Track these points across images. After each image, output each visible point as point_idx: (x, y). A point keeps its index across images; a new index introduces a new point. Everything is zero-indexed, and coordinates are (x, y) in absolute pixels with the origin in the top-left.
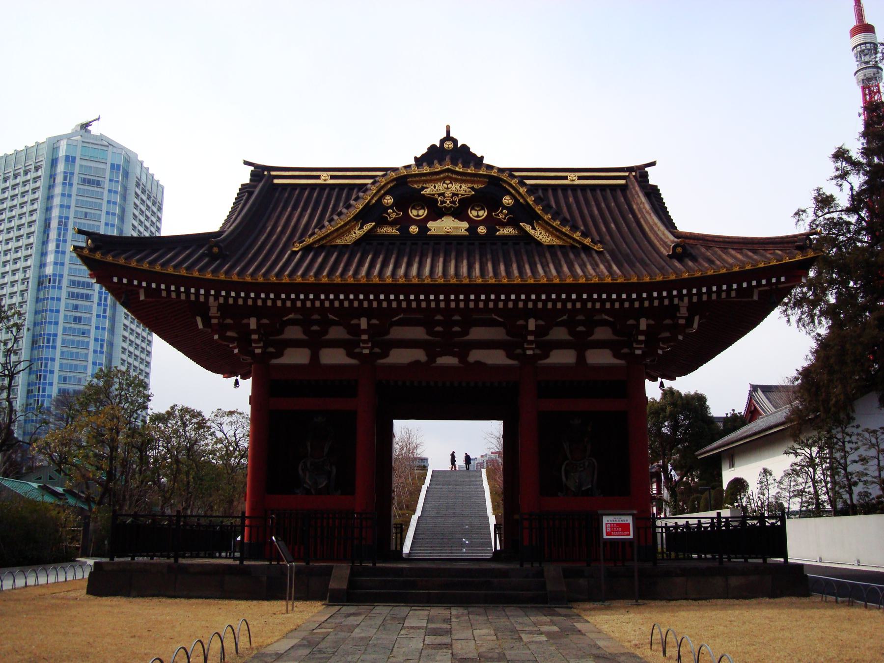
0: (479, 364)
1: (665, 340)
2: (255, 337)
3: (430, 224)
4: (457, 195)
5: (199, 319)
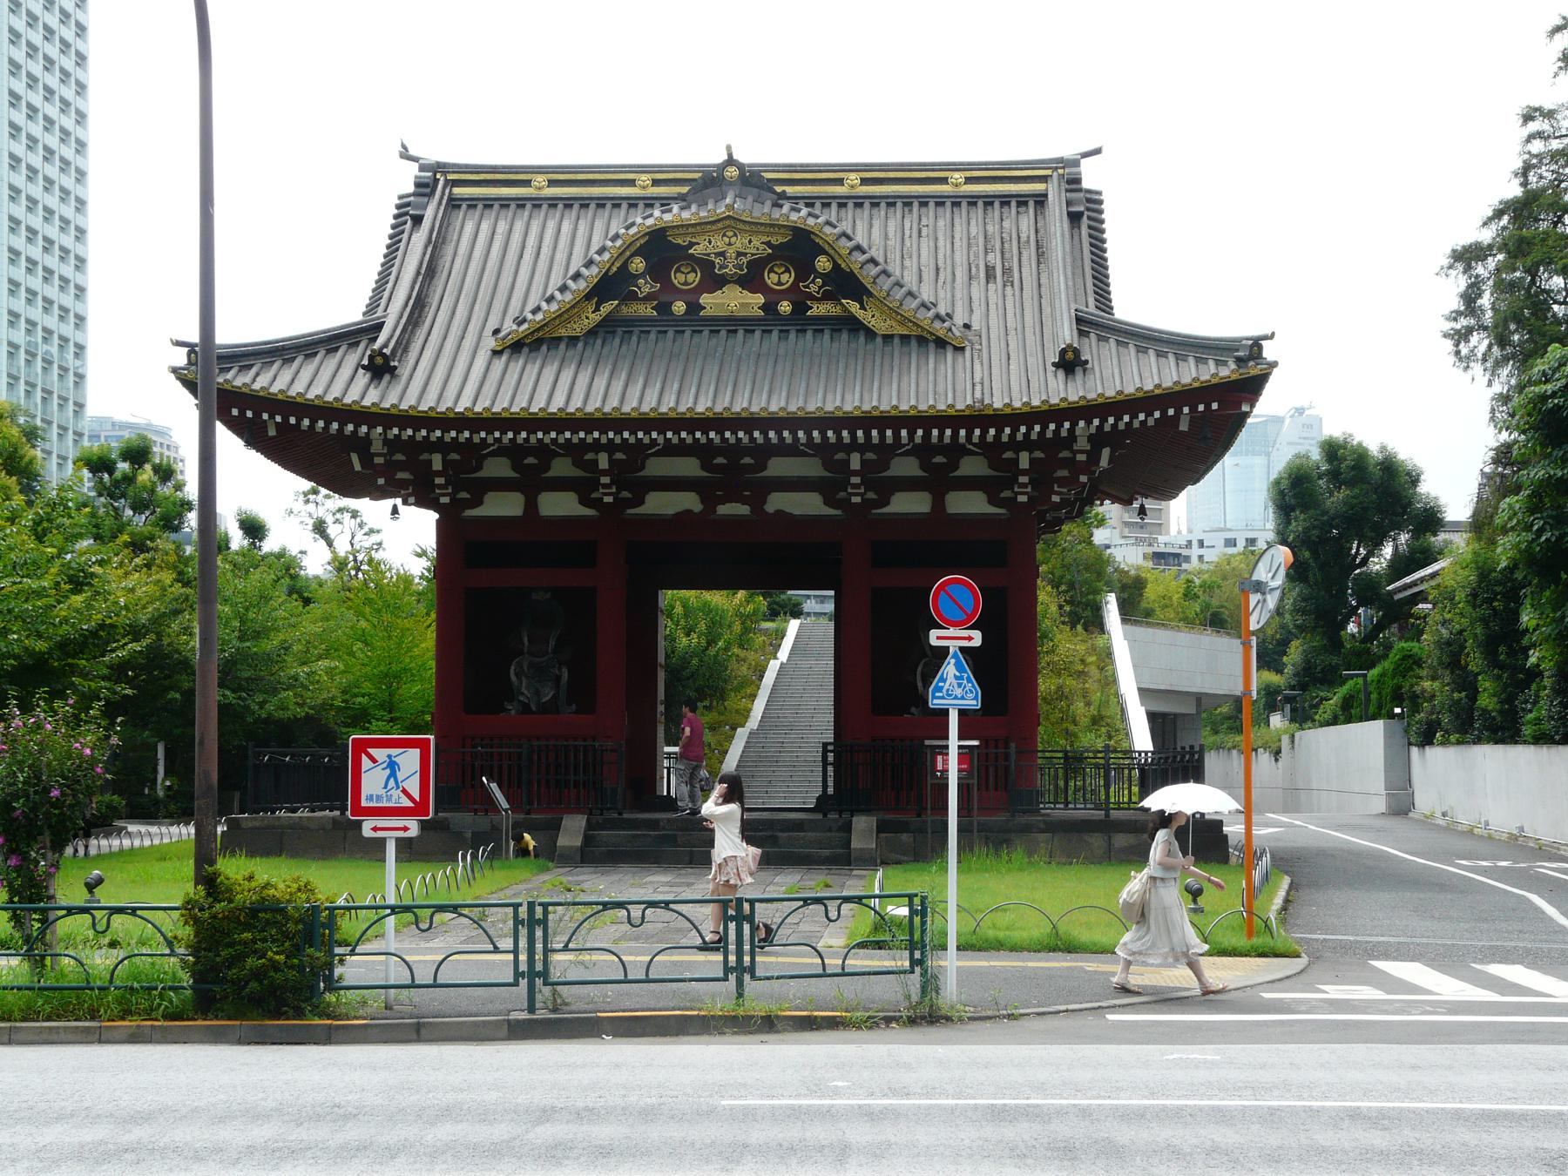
0: (780, 513)
1: (1062, 482)
2: (439, 481)
3: (705, 299)
4: (745, 254)
5: (355, 458)
